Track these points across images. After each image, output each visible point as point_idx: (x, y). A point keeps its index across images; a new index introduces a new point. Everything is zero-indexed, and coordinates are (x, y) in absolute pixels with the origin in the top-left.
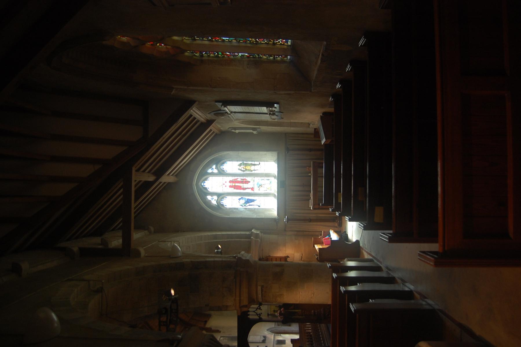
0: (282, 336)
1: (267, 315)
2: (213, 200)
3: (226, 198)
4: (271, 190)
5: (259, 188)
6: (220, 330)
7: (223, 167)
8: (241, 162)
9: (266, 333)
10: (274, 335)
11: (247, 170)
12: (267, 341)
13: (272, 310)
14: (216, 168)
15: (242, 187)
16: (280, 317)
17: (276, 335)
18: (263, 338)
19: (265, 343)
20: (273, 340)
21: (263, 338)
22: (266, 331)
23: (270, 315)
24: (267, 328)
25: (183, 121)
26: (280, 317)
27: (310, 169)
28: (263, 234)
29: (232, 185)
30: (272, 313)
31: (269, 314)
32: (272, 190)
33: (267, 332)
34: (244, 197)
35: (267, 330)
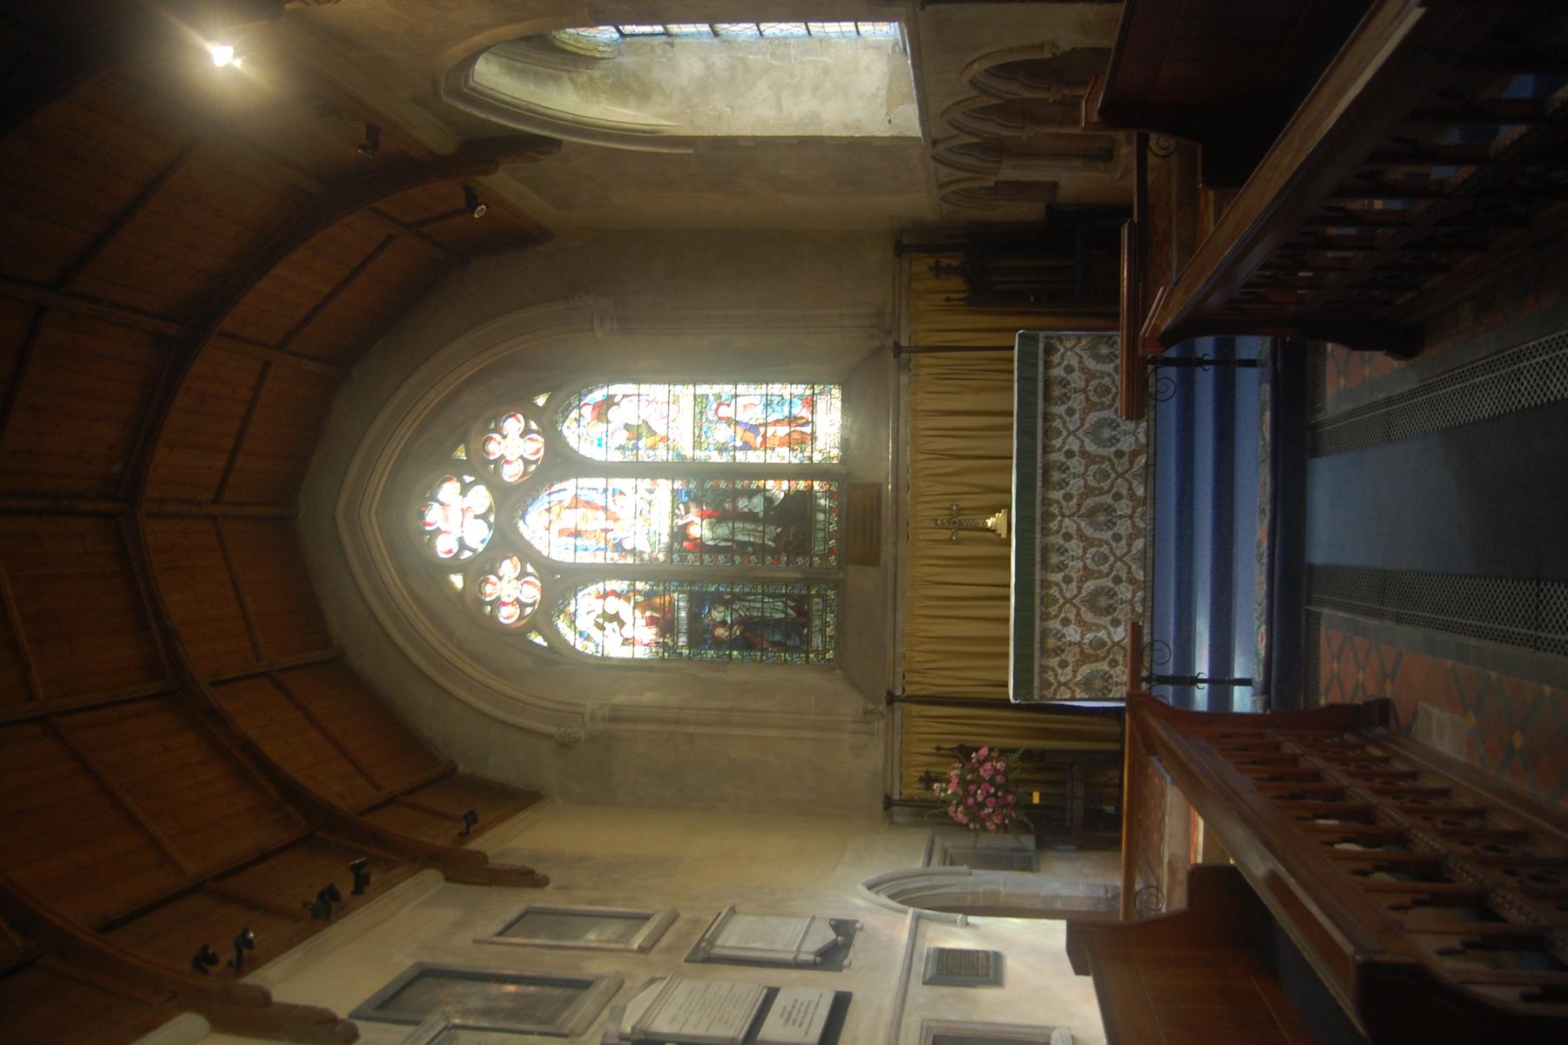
0: (975, 926)
1: (880, 807)
2: (746, 510)
6: (540, 870)
9: (860, 902)
10: (918, 919)
12: (855, 956)
13: (915, 773)
16: (961, 809)
17: (929, 918)
18: (831, 935)
19: (840, 969)
20: (901, 953)
21: (831, 935)
22: (862, 889)
23: (904, 803)
24: (872, 876)
26: (967, 807)
30: (916, 791)
31: (896, 797)
32: (818, 995)
33: (857, 908)
35: (870, 888)
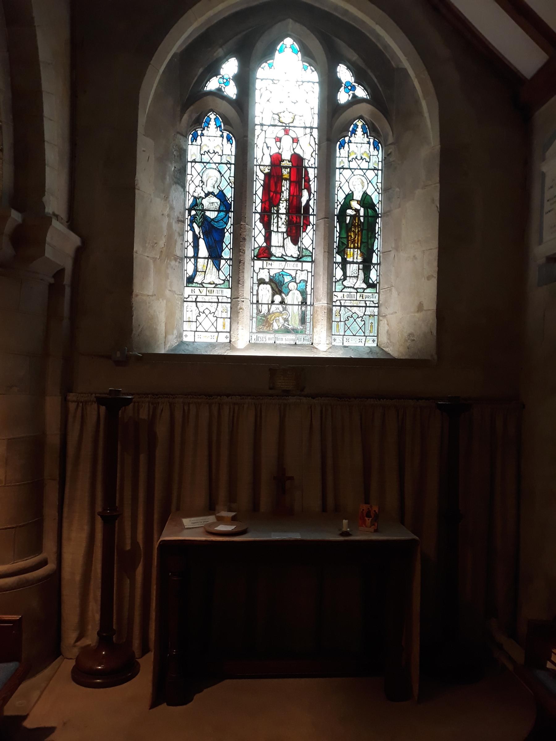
3: (229, 139)
4: (279, 80)
5: (267, 280)
7: (359, 131)
8: (379, 208)
11: (343, 232)
14: (355, 100)
15: (274, 210)
25: (76, 602)
27: (368, 521)
28: (52, 281)
29: (283, 164)
32: (298, 101)
34: (231, 215)
